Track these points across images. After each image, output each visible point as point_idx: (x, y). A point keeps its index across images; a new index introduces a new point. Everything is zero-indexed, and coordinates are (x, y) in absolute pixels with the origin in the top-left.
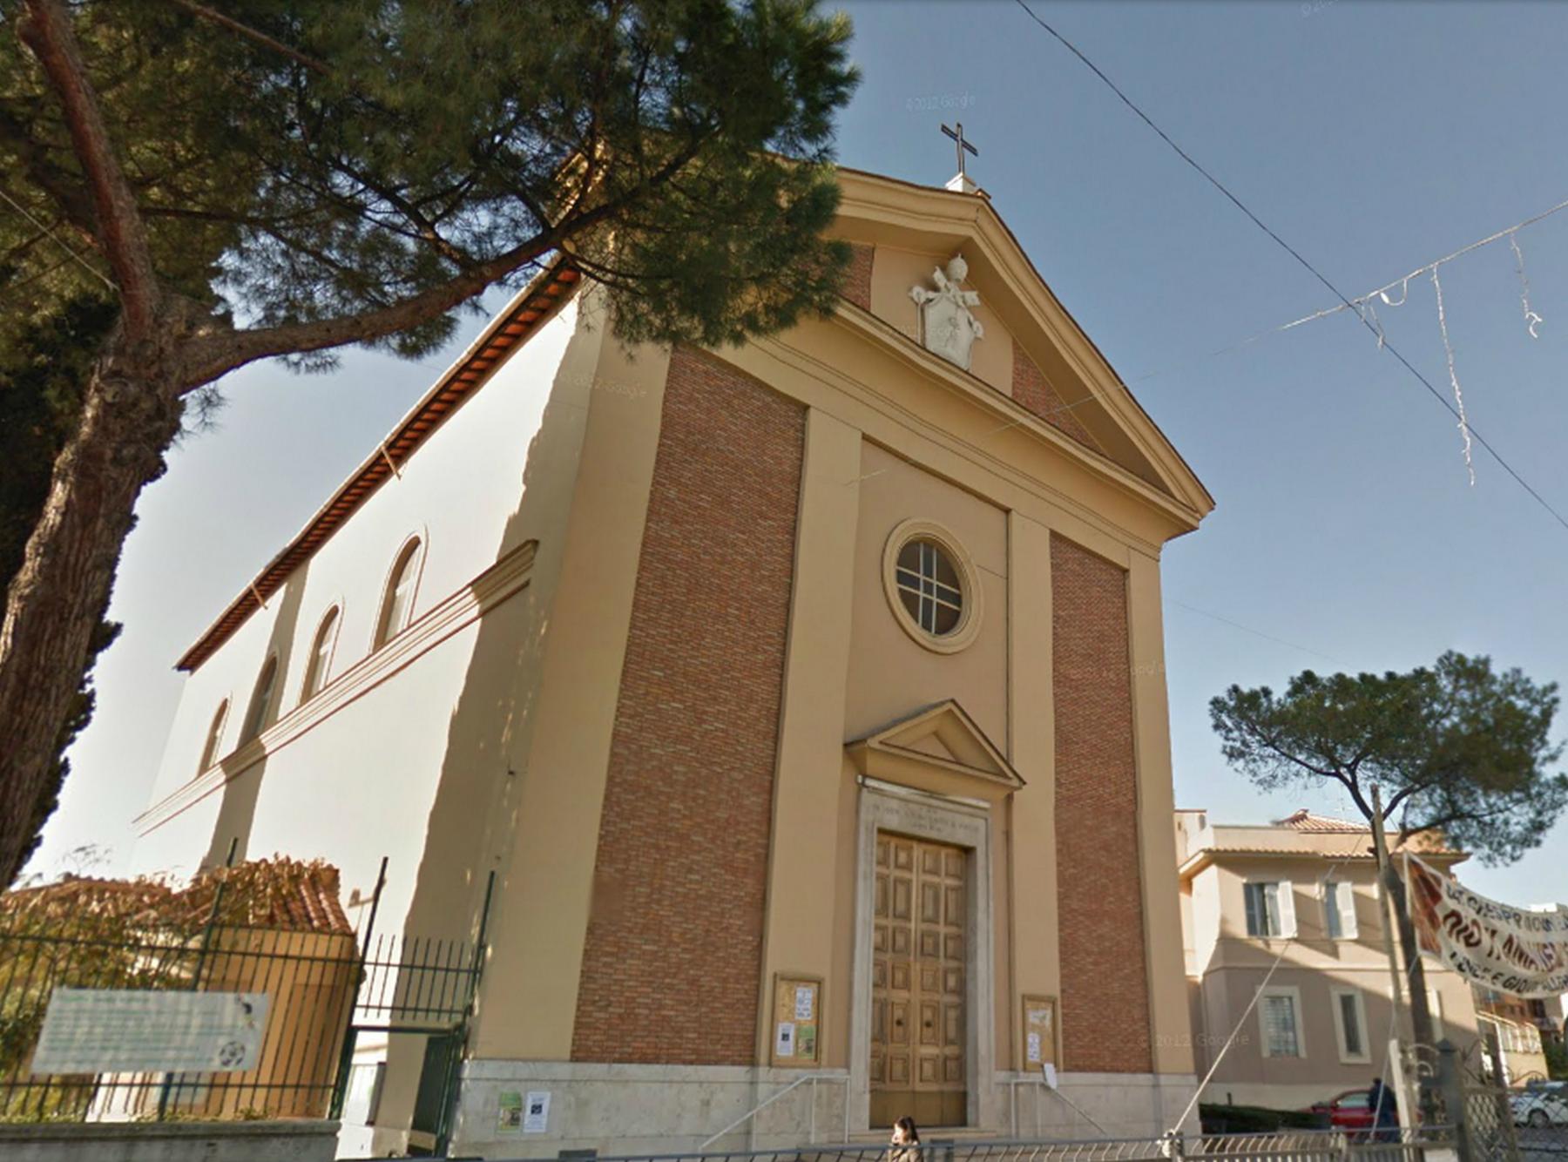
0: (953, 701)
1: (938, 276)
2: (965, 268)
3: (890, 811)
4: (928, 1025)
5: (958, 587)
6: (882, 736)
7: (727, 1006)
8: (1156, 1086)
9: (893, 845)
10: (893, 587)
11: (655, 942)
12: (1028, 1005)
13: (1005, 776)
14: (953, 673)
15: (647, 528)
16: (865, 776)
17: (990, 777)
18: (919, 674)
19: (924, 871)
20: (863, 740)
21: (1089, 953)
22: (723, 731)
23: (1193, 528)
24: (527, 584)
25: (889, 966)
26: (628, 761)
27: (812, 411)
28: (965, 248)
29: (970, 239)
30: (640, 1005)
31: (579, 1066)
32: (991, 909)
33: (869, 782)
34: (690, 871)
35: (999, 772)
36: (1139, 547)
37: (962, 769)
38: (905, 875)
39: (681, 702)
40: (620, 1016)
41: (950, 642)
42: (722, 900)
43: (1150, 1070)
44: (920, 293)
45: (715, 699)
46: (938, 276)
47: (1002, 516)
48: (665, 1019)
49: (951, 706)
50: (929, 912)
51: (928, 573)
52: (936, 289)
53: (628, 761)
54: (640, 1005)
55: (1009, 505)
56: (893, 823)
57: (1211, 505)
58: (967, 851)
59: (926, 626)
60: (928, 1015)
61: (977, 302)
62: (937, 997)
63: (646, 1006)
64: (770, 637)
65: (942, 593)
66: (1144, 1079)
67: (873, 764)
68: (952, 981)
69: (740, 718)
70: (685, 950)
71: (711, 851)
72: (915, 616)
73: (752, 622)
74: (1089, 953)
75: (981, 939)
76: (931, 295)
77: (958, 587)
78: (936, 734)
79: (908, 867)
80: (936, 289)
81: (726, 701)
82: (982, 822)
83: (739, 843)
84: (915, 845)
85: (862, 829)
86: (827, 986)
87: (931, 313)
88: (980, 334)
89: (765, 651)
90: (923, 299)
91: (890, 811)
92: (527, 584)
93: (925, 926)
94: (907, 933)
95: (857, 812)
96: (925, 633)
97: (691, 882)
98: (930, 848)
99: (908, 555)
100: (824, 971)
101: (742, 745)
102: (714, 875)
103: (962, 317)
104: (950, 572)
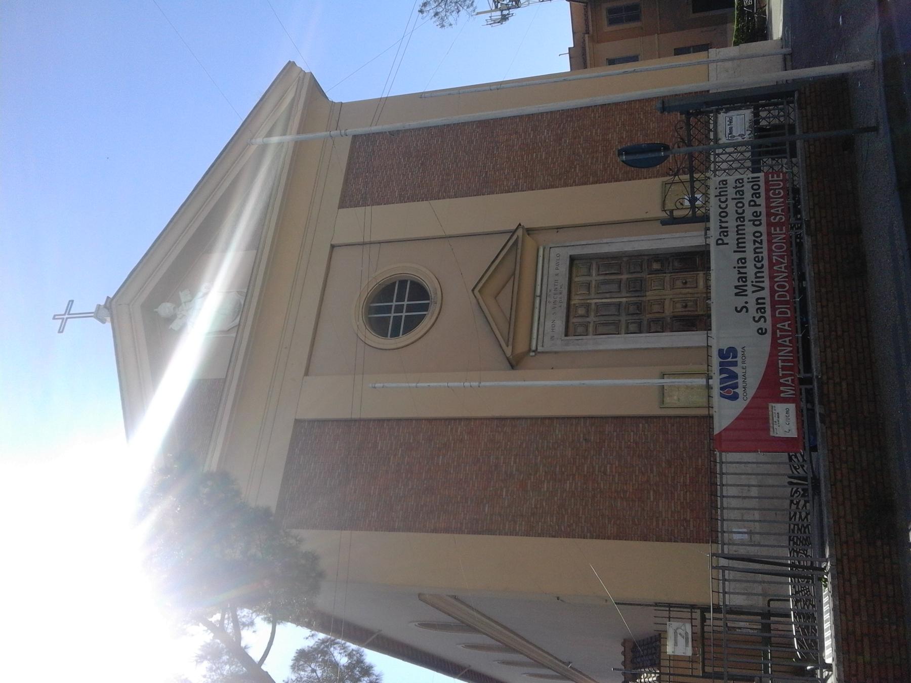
0: (473, 290)
3: (553, 326)
9: (575, 320)
10: (403, 340)
11: (649, 492)
13: (516, 241)
14: (454, 286)
16: (530, 350)
17: (519, 251)
19: (589, 294)
20: (508, 359)
22: (515, 459)
31: (743, 46)
32: (608, 240)
33: (534, 348)
35: (517, 242)
42: (620, 448)
50: (614, 287)
55: (327, 249)
56: (560, 325)
58: (572, 259)
59: (425, 307)
64: (452, 429)
65: (400, 298)
75: (628, 248)
77: (395, 283)
84: (573, 302)
85: (569, 348)
91: (553, 326)
95: (556, 353)
96: (431, 308)
97: (611, 471)
98: (573, 290)
101: (522, 443)
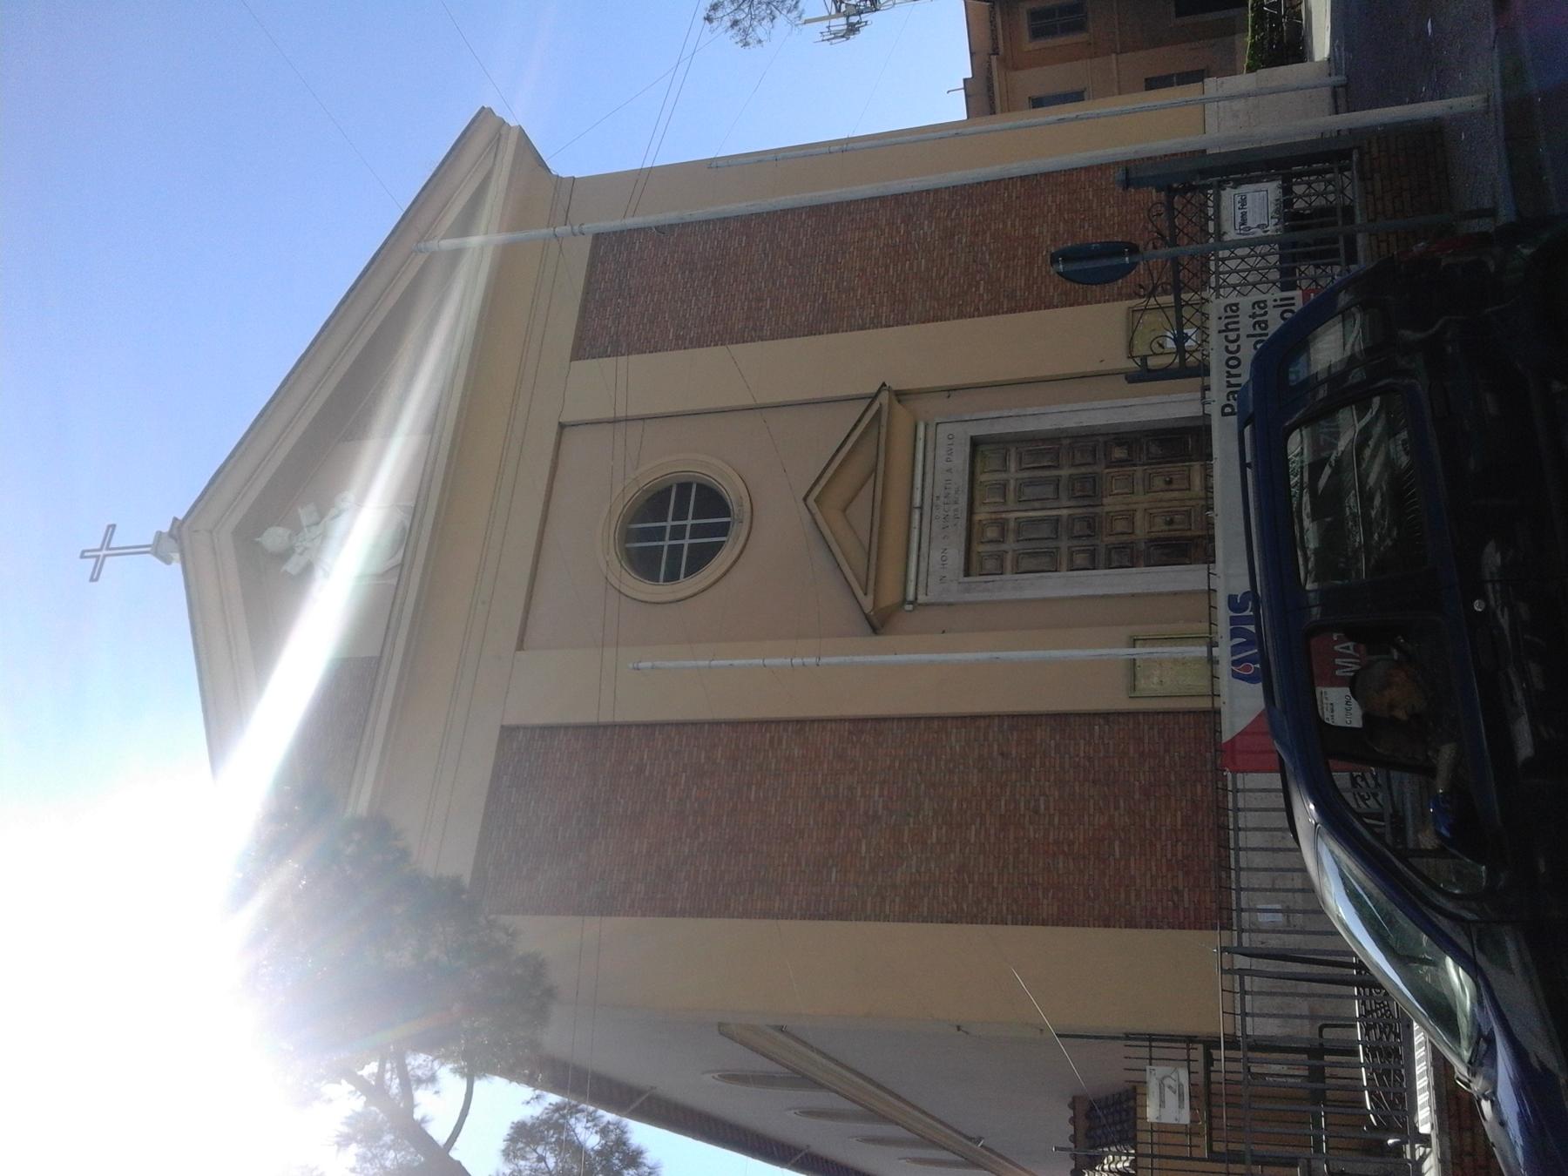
0: (805, 499)
2: (272, 530)
5: (669, 489)
6: (860, 594)
7: (1167, 751)
9: (981, 548)
10: (686, 586)
13: (879, 412)
14: (770, 483)
16: (904, 601)
17: (883, 430)
25: (1113, 539)
33: (911, 597)
35: (879, 415)
37: (881, 466)
49: (811, 500)
55: (555, 428)
56: (956, 557)
57: (484, 114)
58: (975, 443)
59: (724, 530)
64: (772, 739)
67: (889, 597)
70: (1117, 808)
72: (715, 549)
77: (669, 489)
82: (940, 427)
84: (977, 518)
85: (969, 597)
91: (944, 560)
95: (950, 604)
96: (733, 531)
97: (1047, 808)
104: (655, 503)
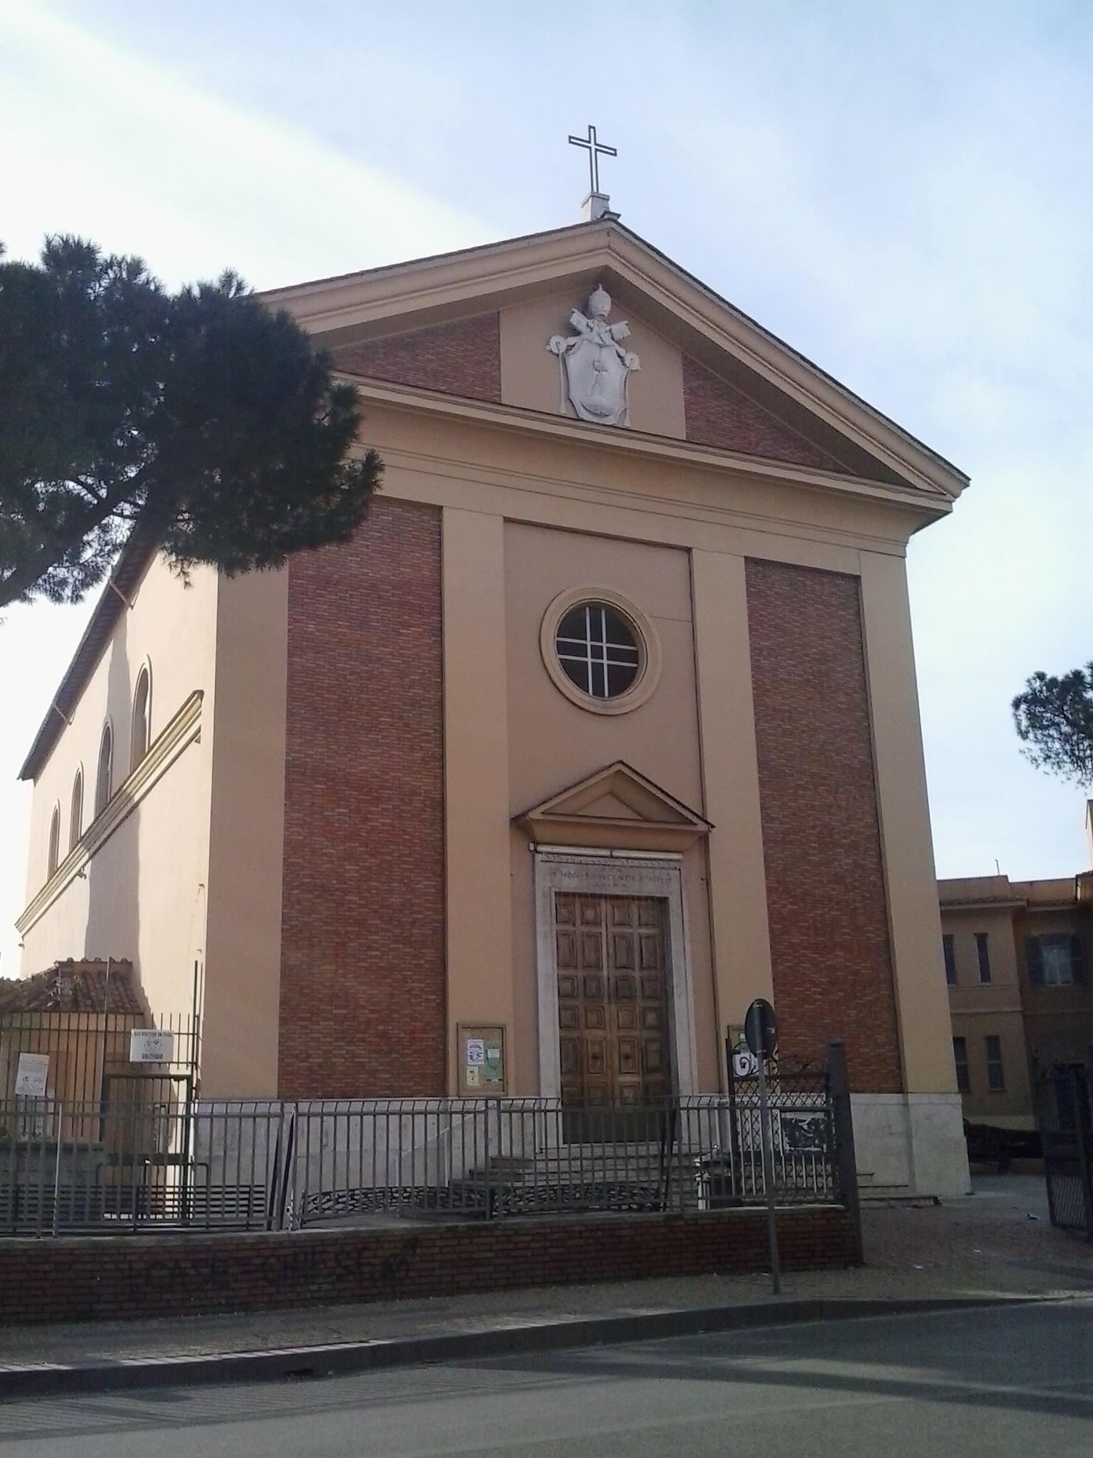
1: (578, 319)
4: (627, 1057)
6: (543, 808)
7: (416, 1051)
8: (906, 1105)
10: (553, 660)
12: (467, 1034)
14: (636, 733)
15: (290, 664)
16: (537, 843)
18: (592, 739)
21: (815, 984)
23: (947, 513)
24: (199, 731)
26: (303, 868)
27: (446, 512)
28: (605, 278)
29: (607, 268)
30: (337, 1056)
33: (540, 848)
34: (370, 948)
36: (869, 546)
38: (595, 930)
39: (346, 807)
40: (320, 1065)
41: (628, 700)
43: (901, 1089)
44: (559, 343)
45: (378, 799)
46: (578, 319)
47: (678, 560)
48: (362, 1065)
49: (620, 767)
51: (597, 636)
52: (576, 332)
53: (303, 868)
54: (337, 1056)
56: (571, 885)
59: (598, 692)
60: (626, 1049)
61: (627, 332)
62: (636, 1033)
63: (342, 1056)
66: (895, 1098)
67: (540, 832)
68: (651, 1018)
69: (404, 811)
70: (372, 1012)
71: (388, 930)
72: (583, 685)
73: (407, 725)
74: (815, 984)
76: (572, 340)
78: (611, 793)
79: (596, 923)
80: (576, 332)
81: (389, 800)
83: (414, 922)
86: (510, 1031)
87: (574, 362)
88: (636, 366)
89: (422, 749)
90: (563, 348)
92: (199, 731)
93: (620, 973)
94: (598, 979)
96: (597, 701)
97: (372, 957)
99: (571, 625)
100: (502, 1015)
102: (393, 950)
103: (609, 359)
